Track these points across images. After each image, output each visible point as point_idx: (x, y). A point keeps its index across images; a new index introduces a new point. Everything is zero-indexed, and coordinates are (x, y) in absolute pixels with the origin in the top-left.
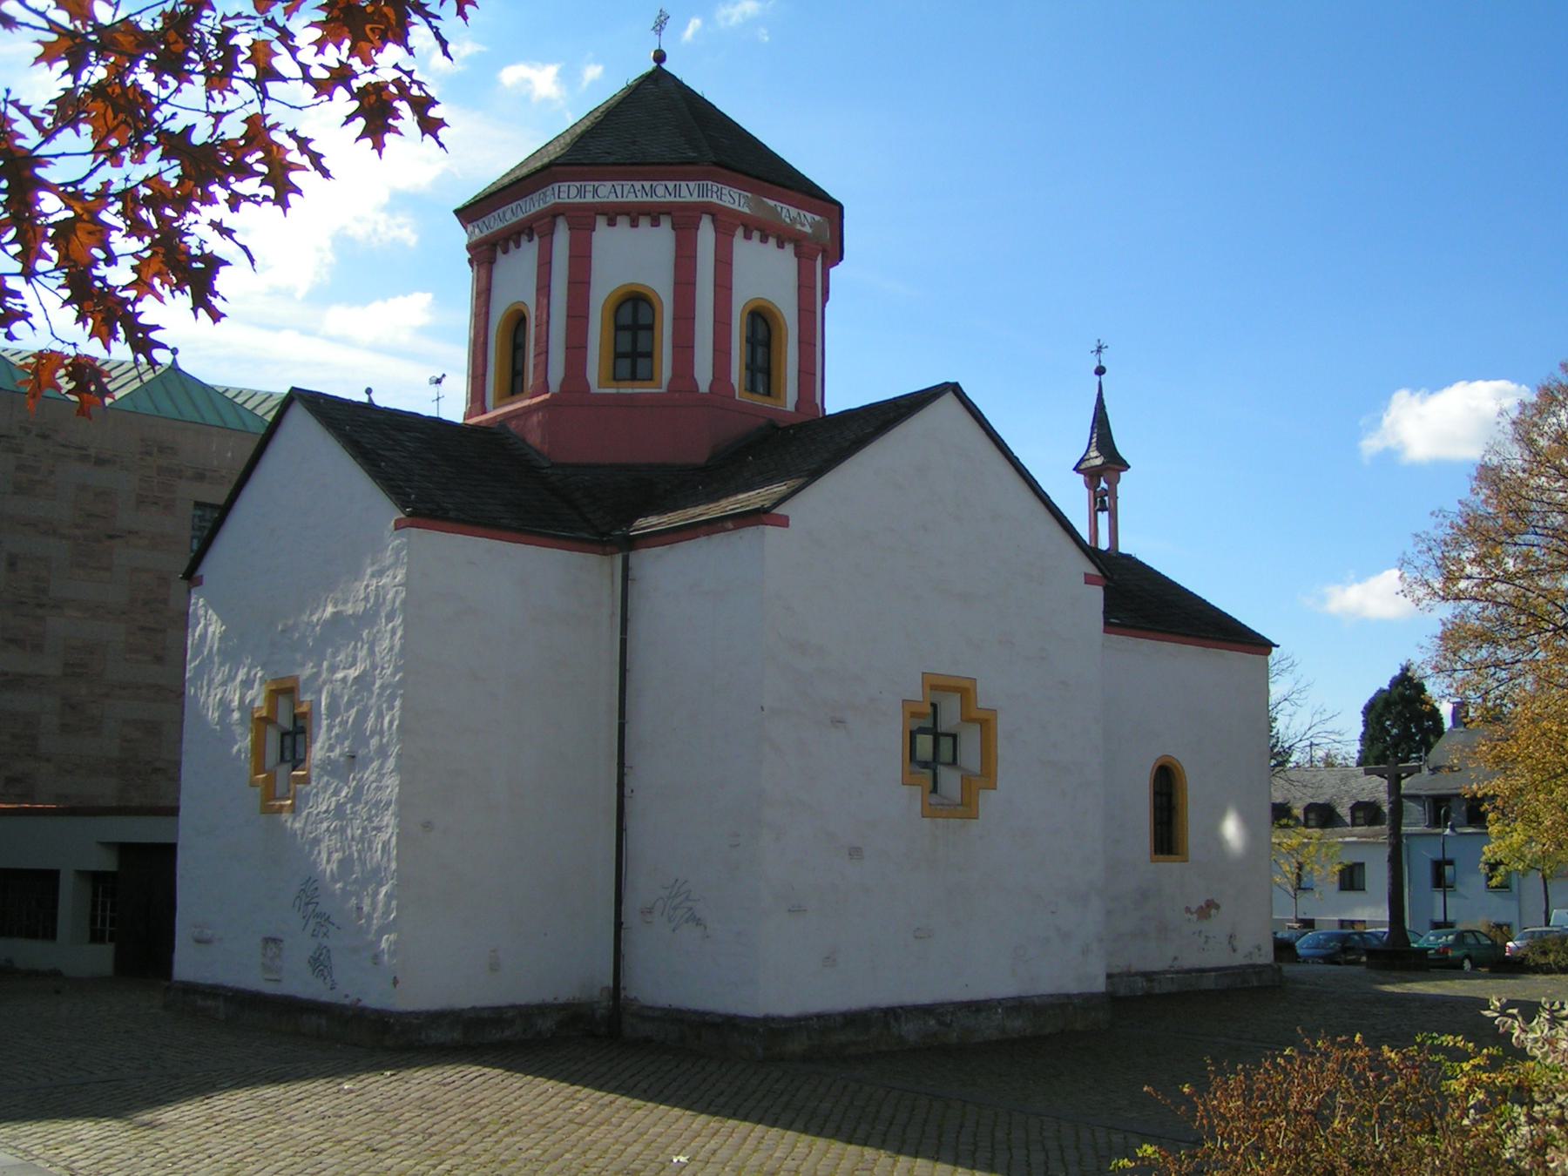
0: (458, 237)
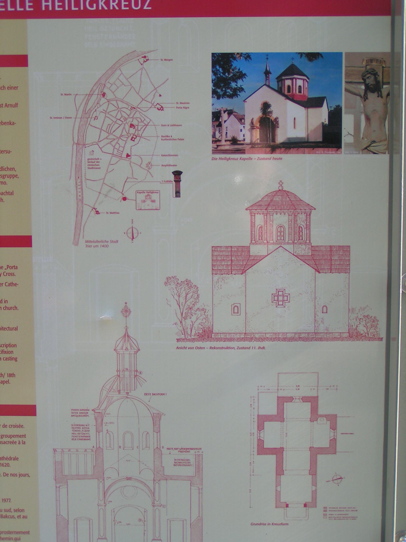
0: (276, 80)
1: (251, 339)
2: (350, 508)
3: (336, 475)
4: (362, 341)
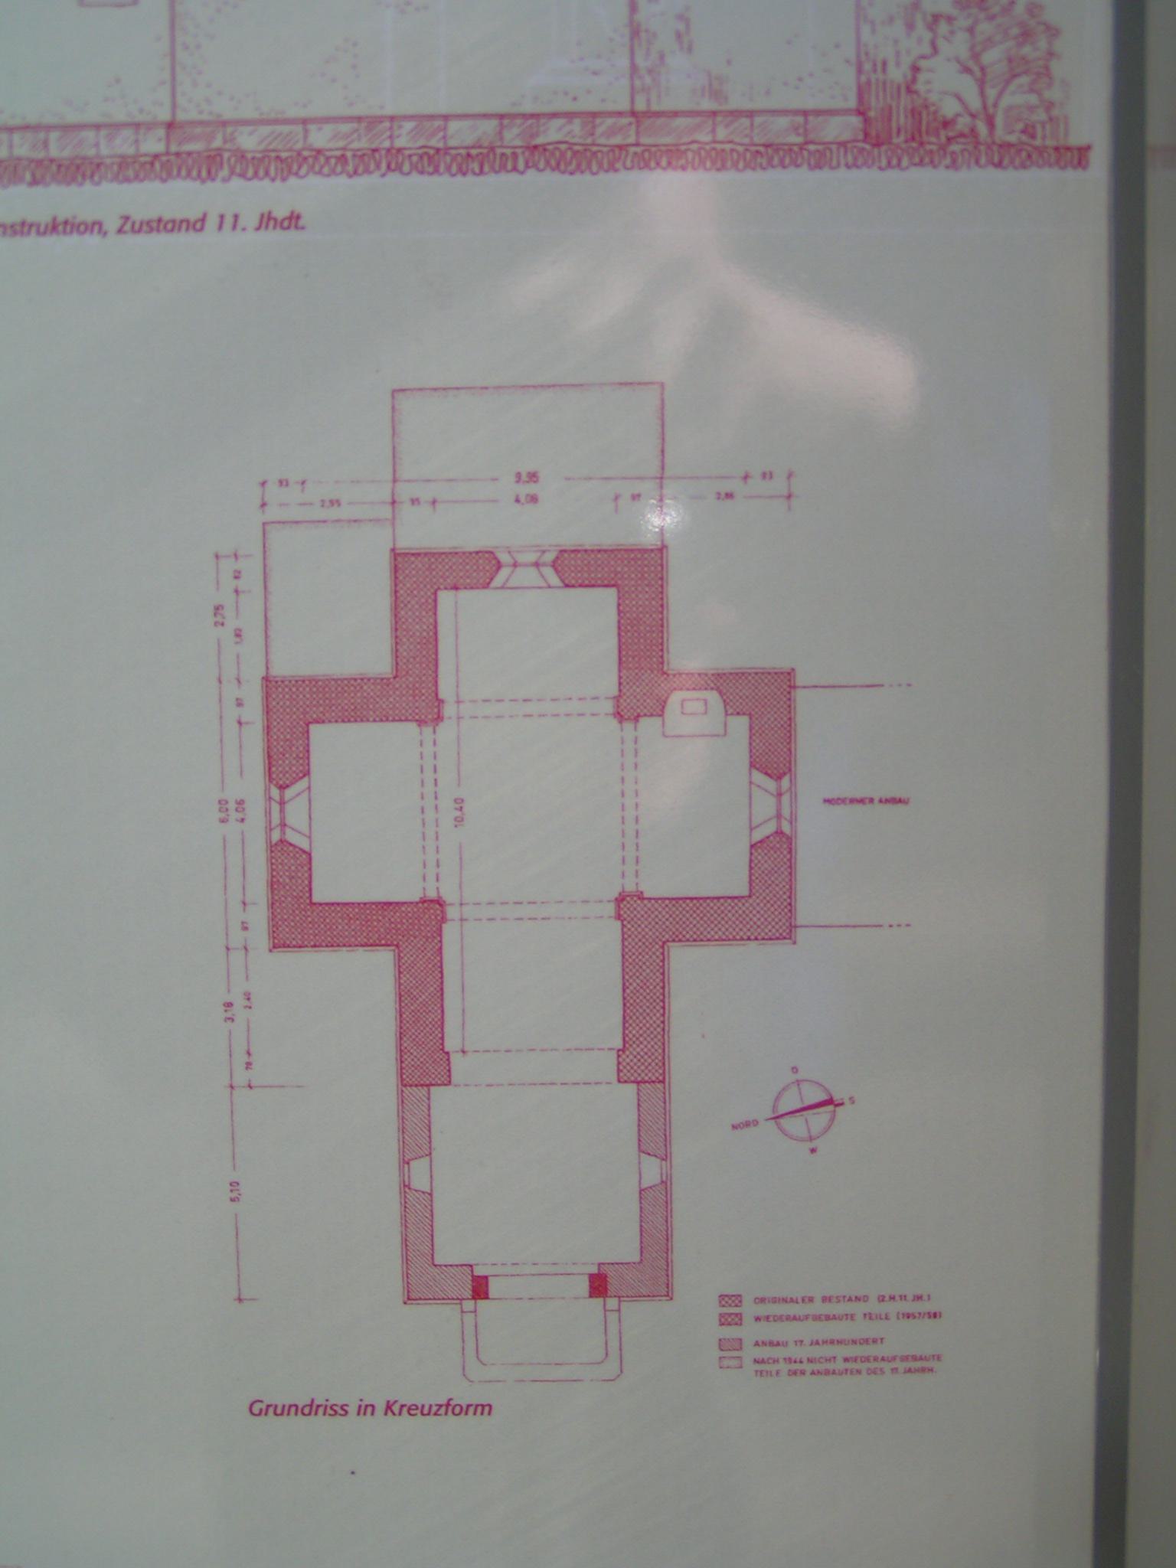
1: (209, 165)
2: (892, 1298)
3: (798, 1082)
4: (954, 165)
